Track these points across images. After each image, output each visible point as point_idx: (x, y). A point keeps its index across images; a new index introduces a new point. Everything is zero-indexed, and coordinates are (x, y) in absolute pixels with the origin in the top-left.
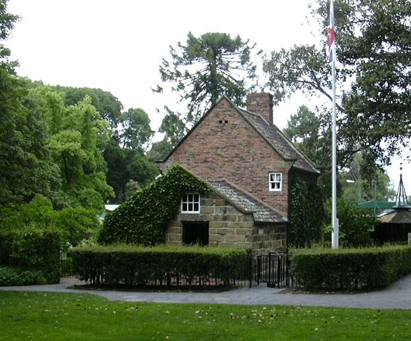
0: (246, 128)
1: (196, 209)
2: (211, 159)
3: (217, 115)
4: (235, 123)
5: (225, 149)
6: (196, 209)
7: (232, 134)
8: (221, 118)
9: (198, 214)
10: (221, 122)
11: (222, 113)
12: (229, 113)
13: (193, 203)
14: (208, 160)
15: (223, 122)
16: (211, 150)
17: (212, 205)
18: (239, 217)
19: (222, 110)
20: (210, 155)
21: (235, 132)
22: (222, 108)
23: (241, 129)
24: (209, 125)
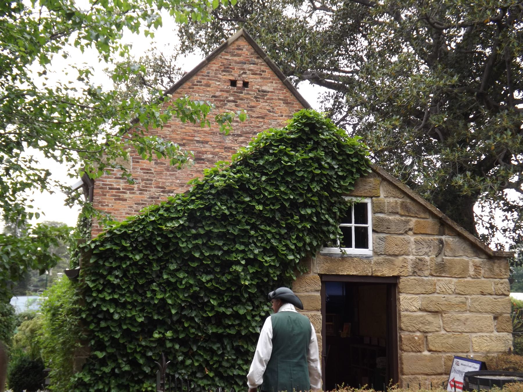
0: (286, 102)
1: (362, 243)
2: (210, 156)
3: (227, 69)
4: (264, 88)
5: (241, 139)
6: (362, 243)
7: (257, 109)
8: (235, 75)
9: (368, 257)
10: (233, 83)
11: (237, 67)
12: (252, 67)
13: (353, 225)
14: (205, 156)
15: (240, 84)
16: (209, 138)
17: (406, 232)
18: (477, 267)
19: (236, 58)
20: (208, 148)
21: (262, 106)
22: (239, 55)
23: (277, 102)
24: (208, 85)
